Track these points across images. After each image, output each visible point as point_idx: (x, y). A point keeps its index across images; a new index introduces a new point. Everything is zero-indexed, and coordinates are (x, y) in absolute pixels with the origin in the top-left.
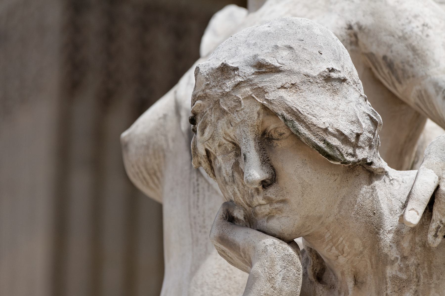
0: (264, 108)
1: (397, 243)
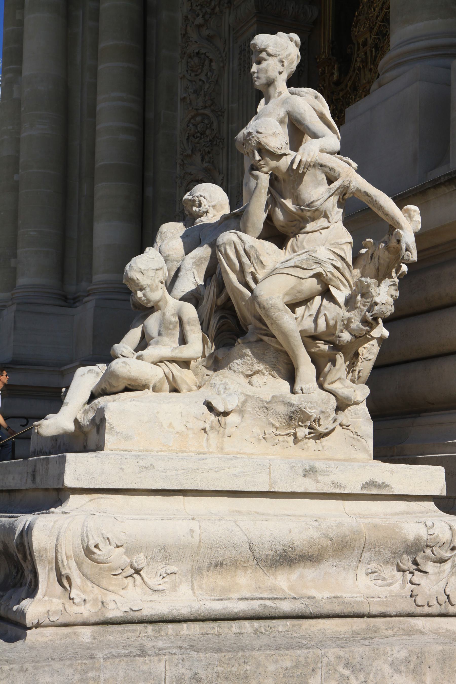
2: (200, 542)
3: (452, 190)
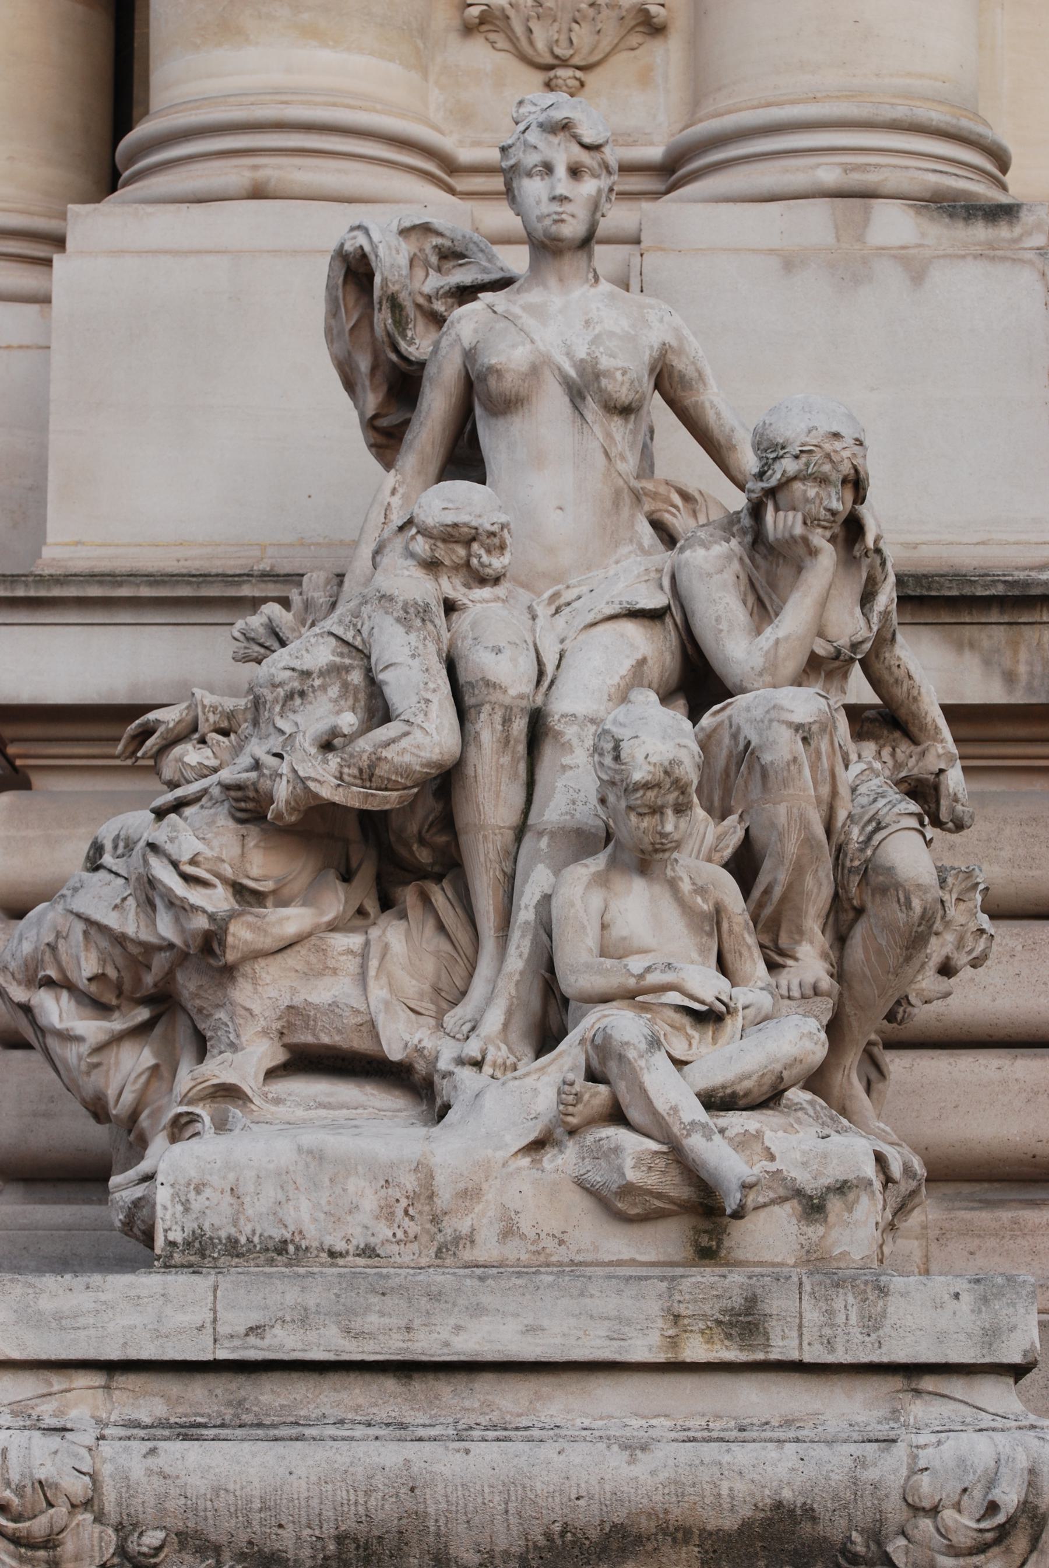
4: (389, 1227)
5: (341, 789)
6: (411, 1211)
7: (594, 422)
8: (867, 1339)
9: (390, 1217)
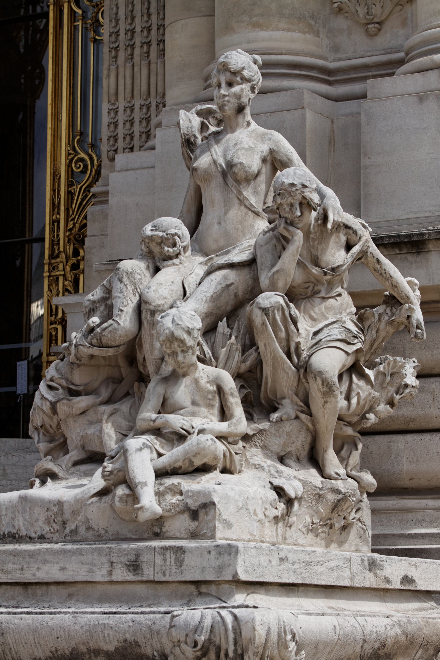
0: (303, 196)
1: (314, 228)
2: (264, 648)
3: (394, 253)
4: (49, 527)
5: (91, 349)
6: (56, 520)
7: (232, 186)
8: (177, 571)
9: (49, 522)
